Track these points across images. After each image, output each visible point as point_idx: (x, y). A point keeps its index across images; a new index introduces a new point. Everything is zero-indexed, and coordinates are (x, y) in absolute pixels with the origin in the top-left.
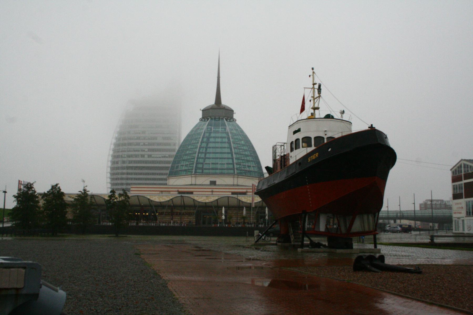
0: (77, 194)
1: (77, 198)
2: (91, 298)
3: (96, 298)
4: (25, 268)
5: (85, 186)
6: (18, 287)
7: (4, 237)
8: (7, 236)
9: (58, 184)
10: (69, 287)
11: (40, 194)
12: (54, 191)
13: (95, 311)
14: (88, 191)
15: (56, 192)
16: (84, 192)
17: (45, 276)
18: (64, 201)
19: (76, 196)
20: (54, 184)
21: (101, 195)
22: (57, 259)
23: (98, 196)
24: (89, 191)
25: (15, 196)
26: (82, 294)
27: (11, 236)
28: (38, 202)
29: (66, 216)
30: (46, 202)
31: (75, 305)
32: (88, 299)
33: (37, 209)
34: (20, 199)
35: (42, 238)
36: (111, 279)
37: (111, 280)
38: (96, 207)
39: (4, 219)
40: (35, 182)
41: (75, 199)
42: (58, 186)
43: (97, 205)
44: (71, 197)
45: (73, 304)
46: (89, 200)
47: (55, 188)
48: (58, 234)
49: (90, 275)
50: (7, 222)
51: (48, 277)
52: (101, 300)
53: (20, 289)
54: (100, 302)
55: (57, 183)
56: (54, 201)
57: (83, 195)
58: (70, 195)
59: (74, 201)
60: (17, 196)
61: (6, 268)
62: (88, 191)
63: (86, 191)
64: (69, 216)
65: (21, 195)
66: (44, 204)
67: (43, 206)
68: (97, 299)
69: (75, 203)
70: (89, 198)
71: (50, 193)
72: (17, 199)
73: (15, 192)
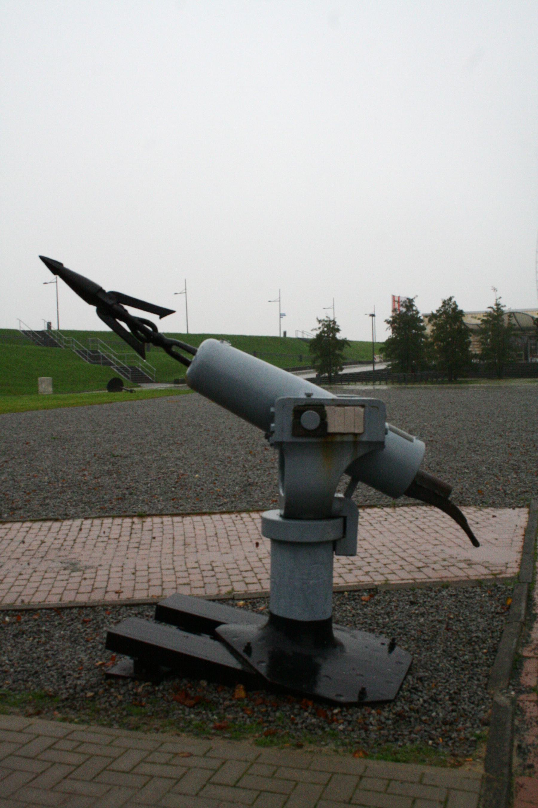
0: (486, 312)
1: (485, 318)
2: (499, 474)
3: (507, 473)
4: (363, 406)
5: (498, 298)
6: (356, 431)
7: (376, 385)
8: (380, 384)
9: (453, 297)
10: (467, 457)
11: (426, 316)
12: (447, 309)
13: (502, 491)
14: (502, 306)
15: (451, 310)
16: (497, 308)
17: (432, 441)
18: (464, 324)
19: (484, 316)
20: (446, 298)
21: (527, 311)
22: (453, 416)
23: (522, 313)
24: (505, 306)
25: (388, 322)
26: (486, 468)
27: (387, 384)
28: (424, 328)
29: (470, 349)
30: (435, 328)
31: (473, 482)
32: (493, 474)
33: (423, 340)
34: (396, 325)
35: (432, 386)
36: (534, 446)
37: (535, 448)
38: (519, 332)
39: (374, 358)
40: (417, 296)
41: (483, 320)
42: (453, 300)
43: (522, 329)
44: (475, 318)
45: (471, 481)
46: (506, 321)
47: (449, 304)
48: (458, 379)
49: (502, 440)
50: (380, 362)
51: (436, 442)
52: (515, 476)
53: (360, 434)
54: (513, 480)
55: (451, 296)
56: (448, 326)
57: (496, 314)
58: (474, 315)
59: (481, 324)
60: (390, 321)
61: (339, 405)
62: (502, 306)
63: (500, 306)
64: (476, 349)
65: (396, 318)
66: (433, 331)
67: (432, 334)
68: (508, 475)
69: (483, 326)
70: (505, 317)
71: (441, 312)
72: (391, 325)
73: (388, 314)
